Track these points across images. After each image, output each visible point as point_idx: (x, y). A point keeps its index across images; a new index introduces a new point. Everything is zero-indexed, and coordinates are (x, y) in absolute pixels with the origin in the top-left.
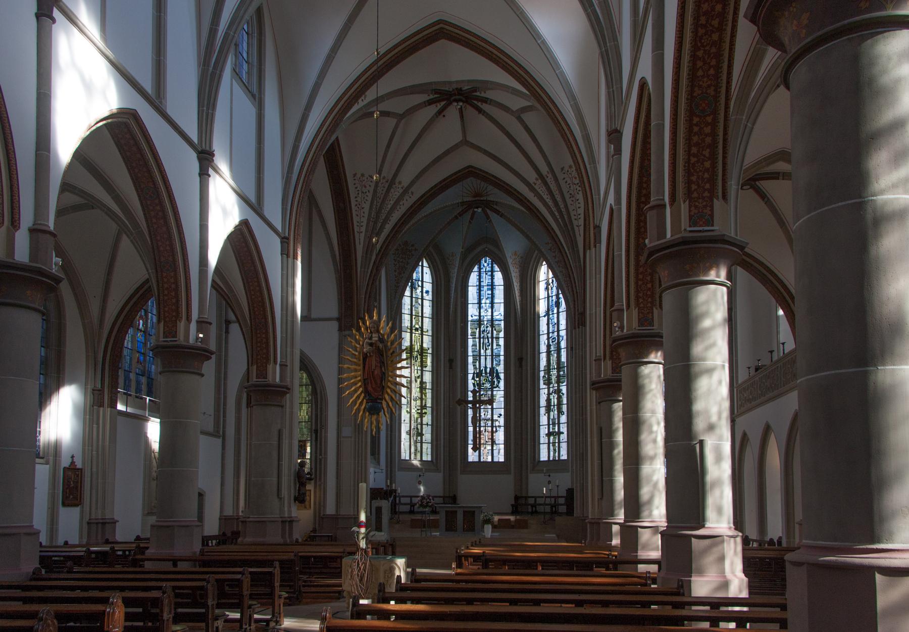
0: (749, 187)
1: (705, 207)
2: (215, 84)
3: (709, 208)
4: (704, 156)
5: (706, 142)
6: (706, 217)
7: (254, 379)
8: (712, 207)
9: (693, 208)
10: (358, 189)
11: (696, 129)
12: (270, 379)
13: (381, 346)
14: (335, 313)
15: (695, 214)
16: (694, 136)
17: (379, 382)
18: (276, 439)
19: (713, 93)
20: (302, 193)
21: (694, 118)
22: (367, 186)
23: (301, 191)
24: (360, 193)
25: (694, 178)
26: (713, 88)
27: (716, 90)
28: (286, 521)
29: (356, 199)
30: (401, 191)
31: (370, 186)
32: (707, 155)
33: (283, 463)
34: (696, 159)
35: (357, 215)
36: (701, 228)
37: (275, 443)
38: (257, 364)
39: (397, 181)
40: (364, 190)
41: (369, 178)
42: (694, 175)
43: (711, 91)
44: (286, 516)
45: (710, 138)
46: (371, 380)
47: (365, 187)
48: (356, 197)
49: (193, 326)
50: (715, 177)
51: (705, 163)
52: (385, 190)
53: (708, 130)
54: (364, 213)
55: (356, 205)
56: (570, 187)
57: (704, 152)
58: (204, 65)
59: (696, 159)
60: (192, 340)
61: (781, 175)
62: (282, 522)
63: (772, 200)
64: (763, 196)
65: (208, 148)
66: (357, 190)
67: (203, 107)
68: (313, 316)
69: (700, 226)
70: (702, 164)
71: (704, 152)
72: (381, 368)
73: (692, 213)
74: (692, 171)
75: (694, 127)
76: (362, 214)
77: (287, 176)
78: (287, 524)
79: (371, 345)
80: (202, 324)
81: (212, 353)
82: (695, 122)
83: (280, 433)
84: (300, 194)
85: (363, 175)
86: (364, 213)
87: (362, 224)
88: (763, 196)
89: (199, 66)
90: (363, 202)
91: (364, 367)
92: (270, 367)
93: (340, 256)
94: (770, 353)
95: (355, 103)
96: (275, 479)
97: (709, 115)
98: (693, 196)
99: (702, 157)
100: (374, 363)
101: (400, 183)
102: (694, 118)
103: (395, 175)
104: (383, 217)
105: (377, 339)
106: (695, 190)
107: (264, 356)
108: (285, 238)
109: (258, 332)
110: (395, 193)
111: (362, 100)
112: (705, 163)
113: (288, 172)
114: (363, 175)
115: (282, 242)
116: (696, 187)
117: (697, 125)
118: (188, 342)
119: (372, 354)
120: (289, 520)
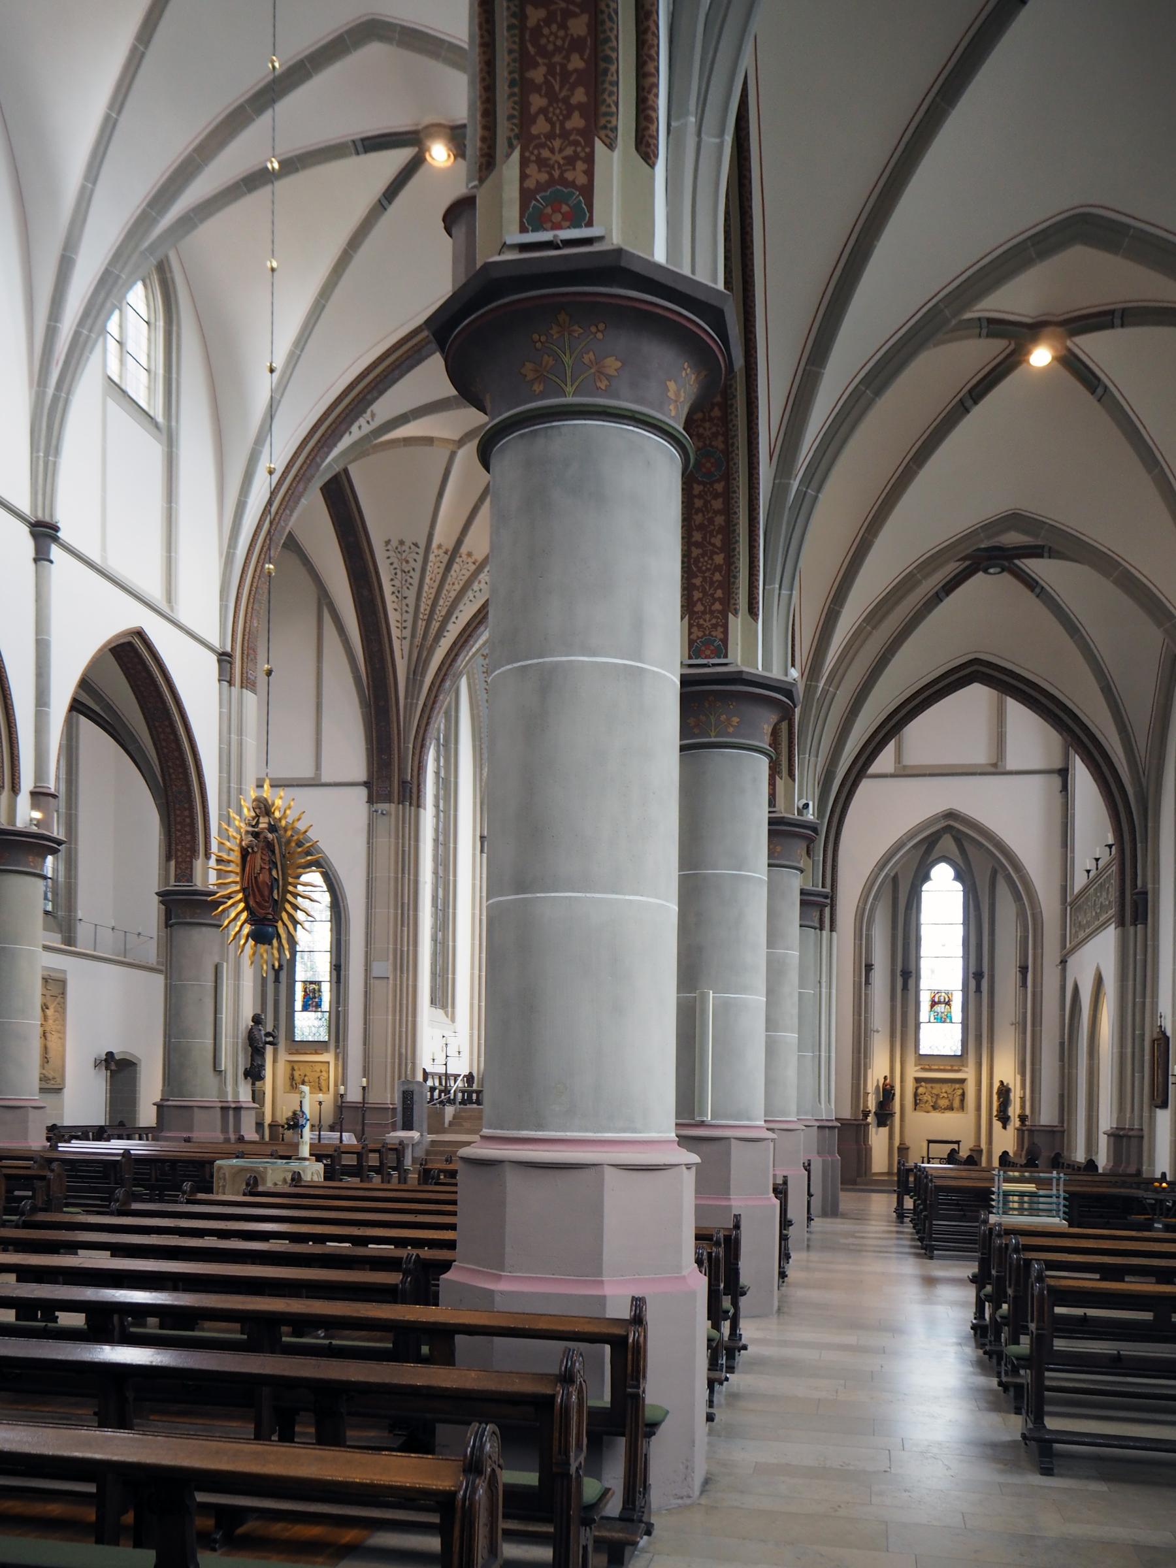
0: (998, 570)
1: (715, 626)
2: (58, 416)
3: (720, 629)
4: (714, 545)
5: (716, 523)
6: (716, 644)
7: (172, 885)
8: (725, 627)
9: (695, 629)
10: (395, 565)
11: (698, 503)
12: (199, 884)
13: (270, 836)
14: (360, 774)
15: (698, 638)
16: (696, 514)
17: (266, 893)
18: (213, 978)
19: (721, 446)
20: (256, 580)
21: (695, 486)
22: (411, 561)
23: (254, 577)
24: (399, 572)
25: (697, 581)
26: (721, 438)
27: (726, 442)
28: (228, 1108)
29: (393, 583)
30: (473, 568)
31: (415, 560)
32: (719, 544)
33: (224, 1016)
34: (700, 551)
35: (396, 610)
36: (704, 661)
37: (211, 984)
38: (177, 858)
39: (464, 550)
40: (406, 568)
41: (413, 547)
42: (697, 576)
43: (719, 443)
44: (230, 1099)
45: (723, 517)
46: (253, 890)
47: (407, 562)
48: (392, 580)
49: (23, 799)
50: (732, 580)
51: (715, 557)
52: (443, 566)
53: (717, 504)
54: (407, 605)
55: (393, 593)
56: (396, 574)
57: (713, 540)
58: (39, 385)
59: (700, 551)
60: (21, 823)
61: (1046, 549)
62: (222, 1108)
63: (1048, 589)
64: (1031, 583)
65: (47, 519)
66: (392, 567)
67: (38, 451)
68: (325, 779)
69: (706, 658)
70: (711, 558)
71: (713, 540)
72: (270, 870)
73: (693, 637)
74: (695, 569)
75: (696, 500)
76: (405, 608)
77: (228, 553)
78: (231, 1113)
79: (256, 835)
80: (39, 796)
81: (60, 843)
82: (696, 492)
83: (217, 969)
84: (252, 582)
85: (402, 543)
86: (407, 605)
87: (404, 625)
88: (1031, 583)
89: (31, 386)
90: (405, 587)
91: (243, 870)
92: (199, 864)
93: (367, 677)
94: (1107, 849)
95: (345, 433)
96: (209, 1042)
97: (718, 481)
98: (696, 609)
99: (711, 548)
100: (258, 862)
101: (469, 554)
102: (695, 486)
103: (459, 542)
104: (443, 613)
105: (265, 826)
106: (700, 600)
107: (188, 846)
108: (224, 654)
109: (177, 806)
110: (460, 572)
111: (360, 427)
112: (715, 557)
113: (229, 547)
114: (402, 543)
115: (219, 661)
116: (701, 595)
117: (700, 496)
118: (14, 824)
119: (256, 849)
120: (233, 1105)
